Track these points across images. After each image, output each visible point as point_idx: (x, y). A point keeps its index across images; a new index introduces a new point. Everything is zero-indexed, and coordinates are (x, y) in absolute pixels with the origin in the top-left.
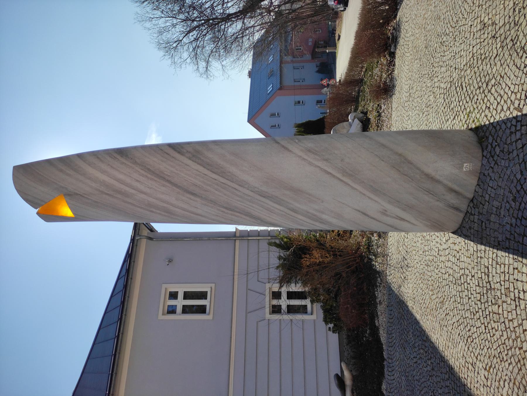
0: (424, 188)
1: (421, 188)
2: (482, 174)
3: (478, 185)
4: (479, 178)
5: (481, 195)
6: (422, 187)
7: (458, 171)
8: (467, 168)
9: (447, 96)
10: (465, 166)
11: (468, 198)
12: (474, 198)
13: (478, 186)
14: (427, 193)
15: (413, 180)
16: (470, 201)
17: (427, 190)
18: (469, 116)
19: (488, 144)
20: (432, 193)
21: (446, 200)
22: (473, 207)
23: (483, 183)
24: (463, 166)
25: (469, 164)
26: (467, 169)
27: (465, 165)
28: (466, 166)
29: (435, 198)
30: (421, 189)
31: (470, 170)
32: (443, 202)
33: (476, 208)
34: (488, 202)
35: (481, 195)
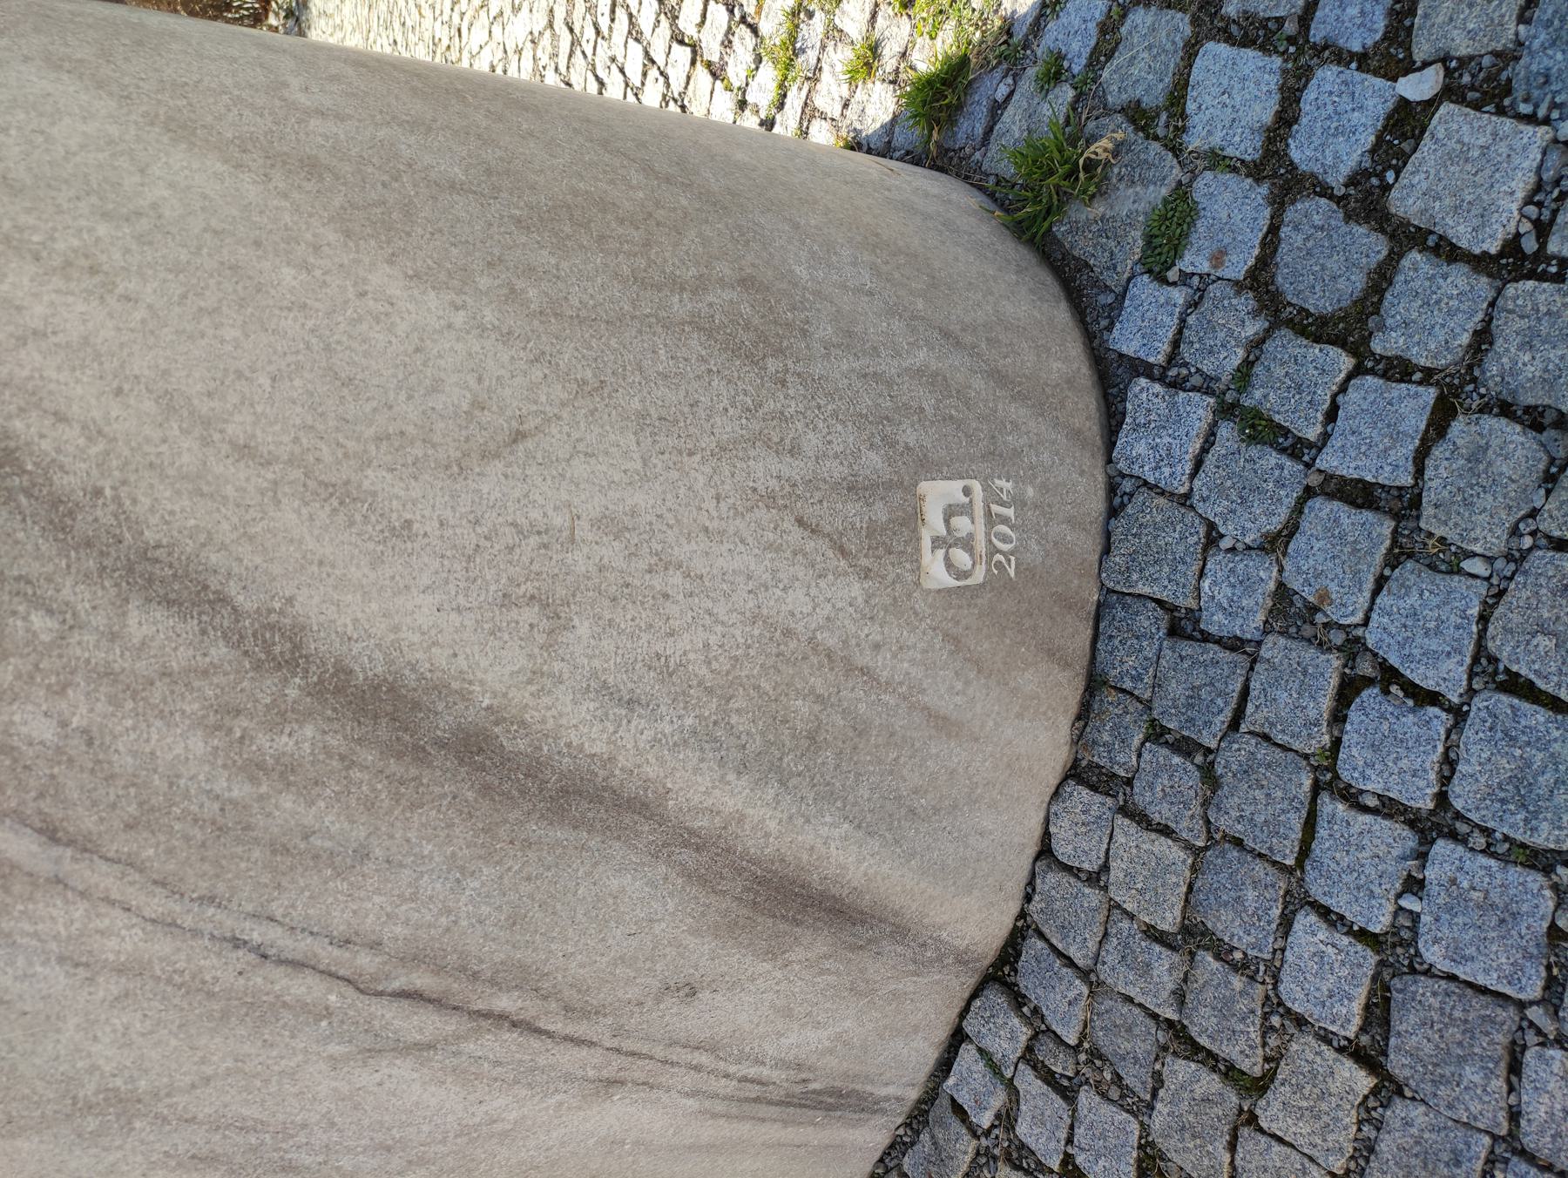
0: (366, 961)
1: (297, 965)
2: (1149, 621)
3: (1075, 773)
4: (1095, 683)
5: (1169, 920)
6: (327, 954)
7: (856, 589)
8: (967, 544)
9: (563, 69)
10: (934, 522)
11: (961, 959)
12: (1034, 946)
13: (1081, 795)
14: (422, 1024)
15: (86, 846)
16: (971, 981)
17: (422, 980)
18: (796, 53)
19: (1182, 193)
20: (504, 1002)
21: (712, 1048)
22: (1028, 1055)
23: (1185, 747)
24: (913, 518)
25: (976, 486)
26: (961, 558)
27: (938, 493)
28: (950, 513)
29: (568, 1058)
30: (303, 987)
31: (997, 584)
32: (690, 1080)
33: (1086, 1098)
34: (1367, 1057)
35: (1169, 920)
